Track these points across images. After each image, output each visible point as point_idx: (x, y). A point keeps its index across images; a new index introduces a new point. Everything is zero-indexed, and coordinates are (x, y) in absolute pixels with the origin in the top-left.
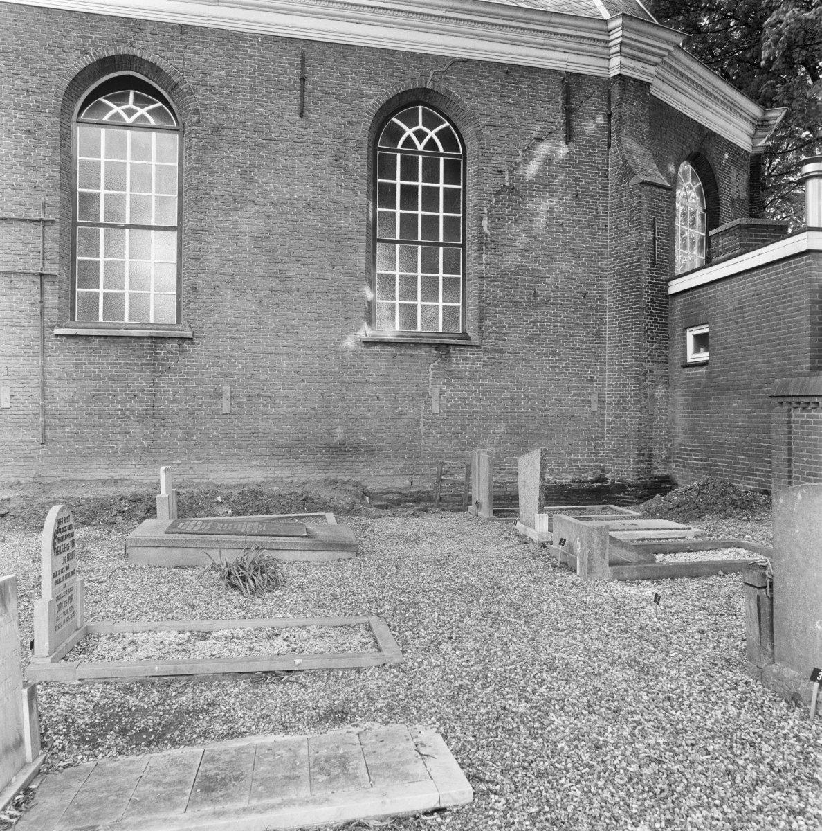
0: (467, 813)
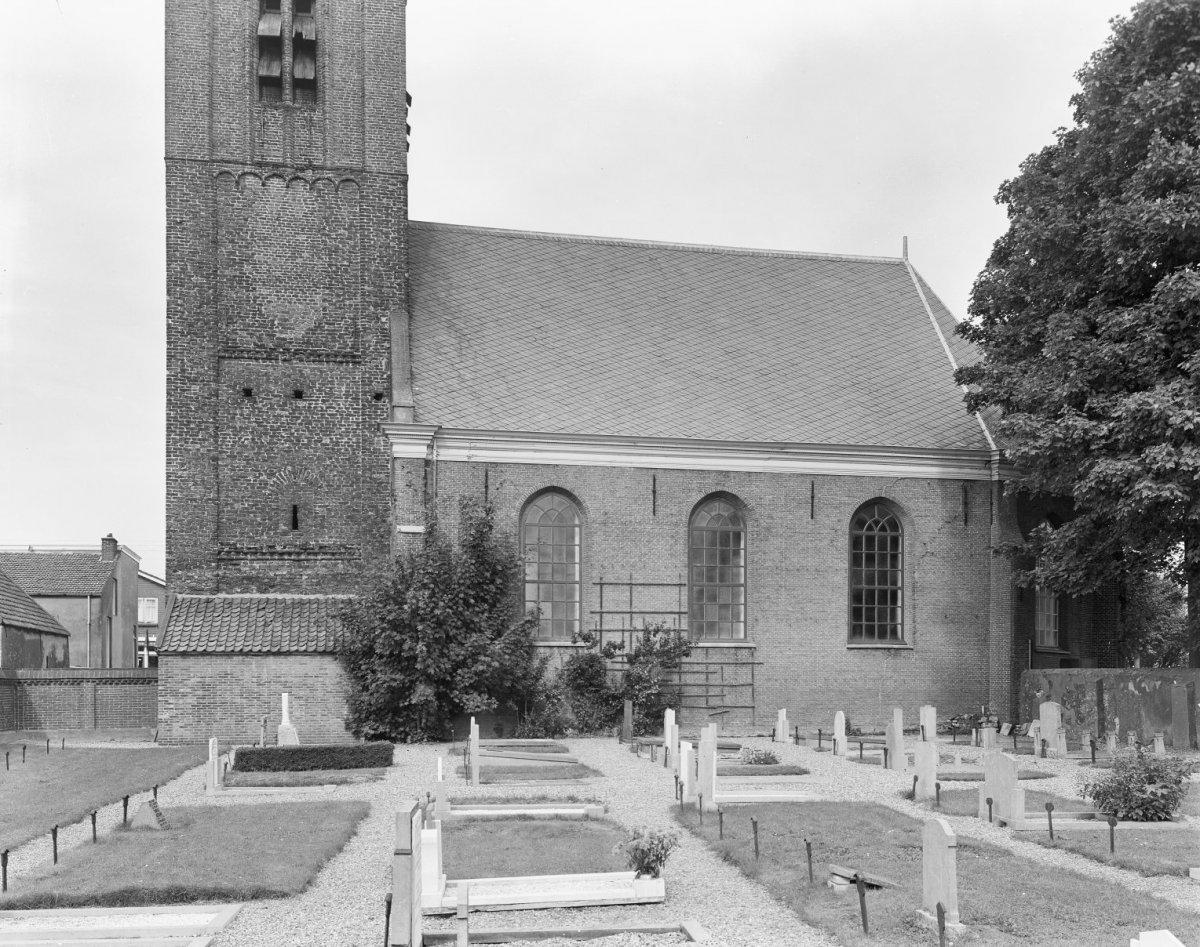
0: (188, 333)
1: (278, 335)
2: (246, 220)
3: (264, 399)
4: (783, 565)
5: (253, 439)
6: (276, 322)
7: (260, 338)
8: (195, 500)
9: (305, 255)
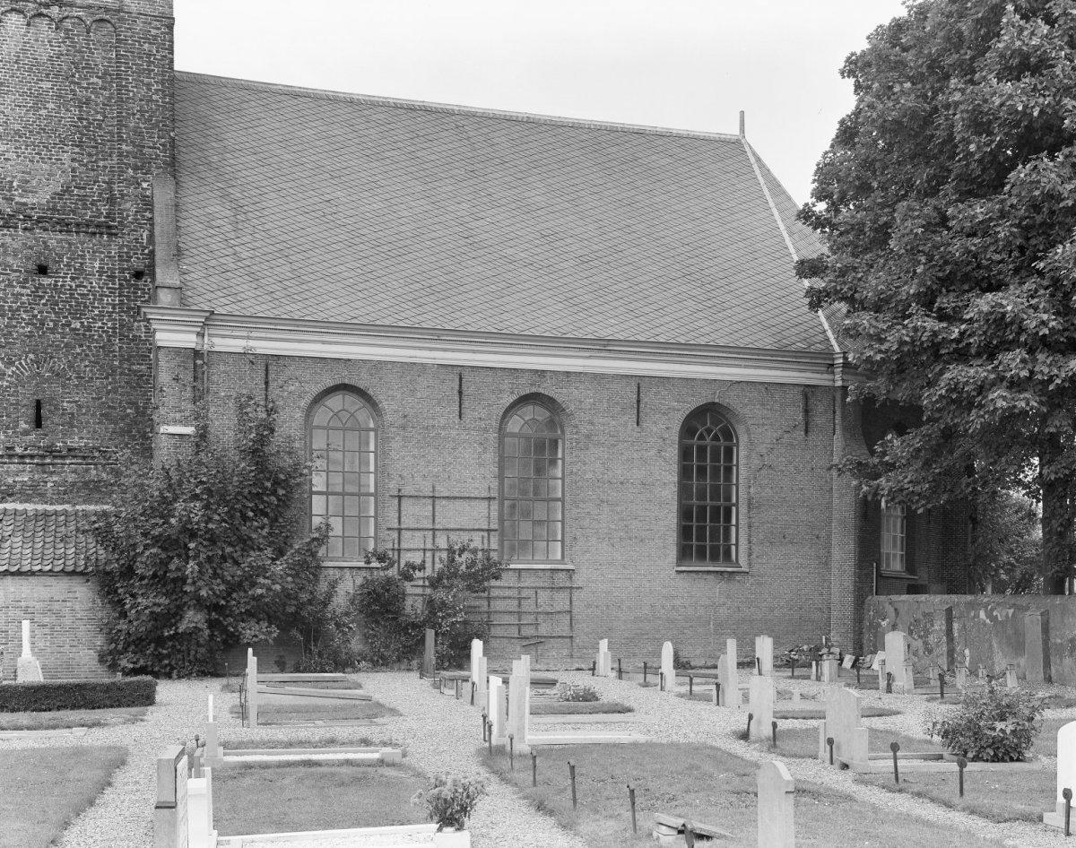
1: (17, 199)
6: (15, 184)
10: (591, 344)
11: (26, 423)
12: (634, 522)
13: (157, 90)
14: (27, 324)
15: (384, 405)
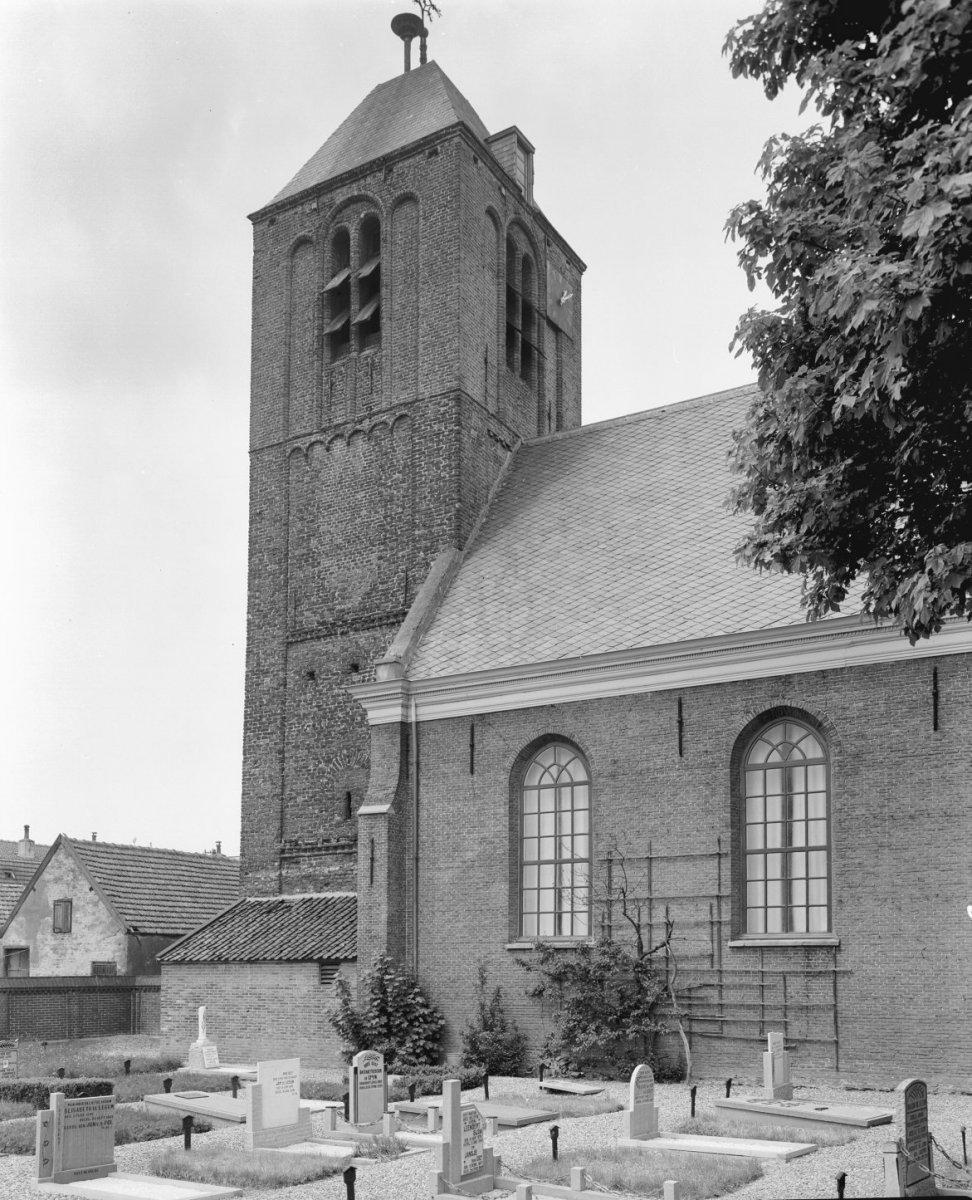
1: (338, 607)
2: (313, 492)
3: (324, 679)
4: (886, 810)
5: (314, 726)
6: (336, 594)
7: (322, 616)
8: (263, 797)
9: (364, 512)
10: (845, 626)
11: (339, 815)
12: (934, 873)
13: (444, 467)
14: (342, 722)
15: (591, 751)
